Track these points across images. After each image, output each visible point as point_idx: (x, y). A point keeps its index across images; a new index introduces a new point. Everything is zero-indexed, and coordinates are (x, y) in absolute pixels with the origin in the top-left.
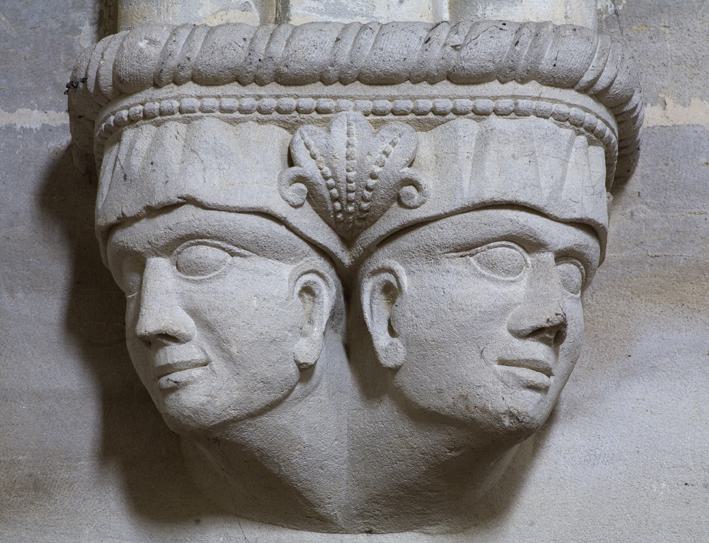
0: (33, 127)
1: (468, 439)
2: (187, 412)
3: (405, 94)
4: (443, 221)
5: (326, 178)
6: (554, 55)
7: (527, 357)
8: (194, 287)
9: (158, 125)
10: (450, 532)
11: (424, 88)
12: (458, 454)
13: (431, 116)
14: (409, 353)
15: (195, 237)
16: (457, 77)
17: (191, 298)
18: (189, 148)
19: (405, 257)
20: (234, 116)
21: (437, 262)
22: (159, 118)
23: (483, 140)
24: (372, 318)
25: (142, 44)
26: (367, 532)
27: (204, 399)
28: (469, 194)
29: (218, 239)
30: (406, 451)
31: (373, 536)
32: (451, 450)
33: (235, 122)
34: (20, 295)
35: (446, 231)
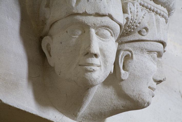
2: (93, 80)
8: (102, 42)
14: (129, 77)
21: (143, 53)
29: (112, 30)
30: (109, 103)
32: (122, 107)
34: (10, 19)
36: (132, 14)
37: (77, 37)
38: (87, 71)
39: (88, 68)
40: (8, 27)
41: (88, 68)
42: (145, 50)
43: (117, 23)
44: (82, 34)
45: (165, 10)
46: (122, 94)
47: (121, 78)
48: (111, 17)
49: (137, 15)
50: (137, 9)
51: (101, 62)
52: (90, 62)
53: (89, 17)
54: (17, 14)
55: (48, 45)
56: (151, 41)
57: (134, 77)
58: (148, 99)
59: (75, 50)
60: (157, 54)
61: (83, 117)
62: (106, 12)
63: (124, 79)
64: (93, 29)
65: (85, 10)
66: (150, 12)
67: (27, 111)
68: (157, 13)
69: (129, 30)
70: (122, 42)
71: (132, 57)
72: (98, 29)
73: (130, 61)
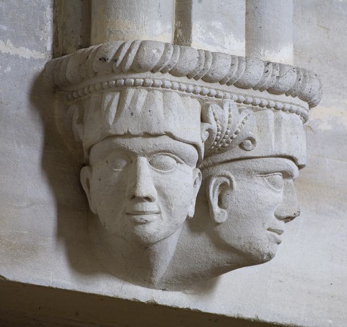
0: (27, 57)
1: (241, 260)
2: (147, 235)
3: (251, 95)
4: (260, 159)
5: (218, 131)
6: (310, 87)
7: (279, 229)
8: (160, 175)
9: (149, 90)
10: (194, 294)
11: (257, 93)
12: (230, 265)
13: (258, 106)
14: (229, 218)
15: (166, 152)
16: (272, 90)
17: (159, 181)
18: (166, 104)
19: (236, 171)
20: (184, 92)
21: (251, 178)
22: (150, 87)
23: (278, 122)
24: (213, 197)
25: (154, 51)
26: (163, 290)
27: (155, 230)
28: (275, 150)
29: (176, 154)
31: (165, 292)
32: (227, 263)
33: (183, 95)
34: (22, 147)
35: (260, 165)
36: (218, 121)
37: (120, 170)
38: (137, 223)
39: (138, 218)
40: (19, 161)
41: (138, 218)
42: (253, 172)
43: (184, 144)
44: (127, 166)
45: (297, 100)
46: (220, 245)
47: (215, 220)
48: (170, 135)
49: (229, 122)
50: (230, 111)
51: (161, 206)
52: (140, 210)
53: (135, 139)
54: (37, 136)
55: (88, 180)
56: (263, 157)
57: (236, 217)
58: (267, 249)
59: (118, 191)
60: (280, 175)
61: (166, 283)
62: (161, 130)
63: (219, 221)
64: (144, 158)
65: (128, 130)
66: (263, 110)
67: (54, 286)
68: (276, 108)
69: (220, 145)
70: (213, 163)
71: (231, 186)
72: (152, 156)
73: (229, 192)
